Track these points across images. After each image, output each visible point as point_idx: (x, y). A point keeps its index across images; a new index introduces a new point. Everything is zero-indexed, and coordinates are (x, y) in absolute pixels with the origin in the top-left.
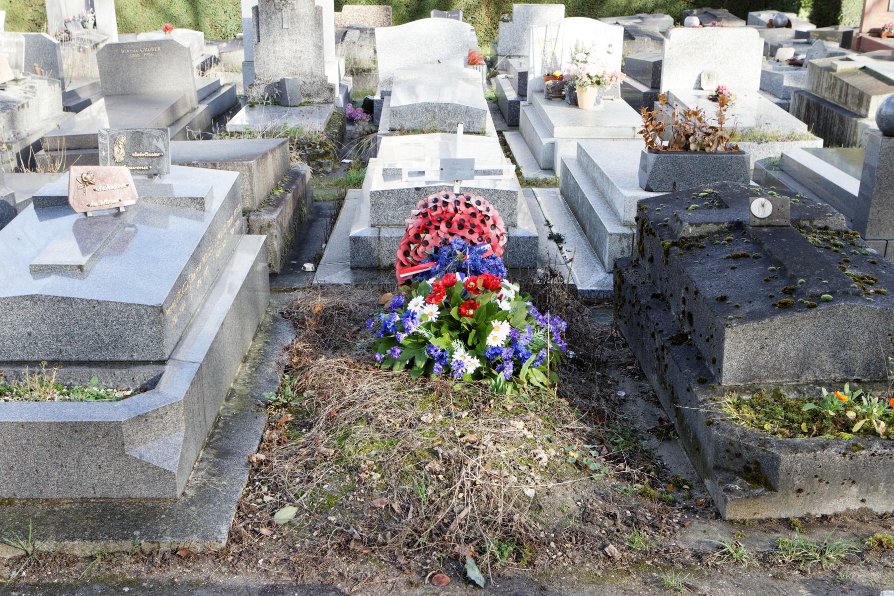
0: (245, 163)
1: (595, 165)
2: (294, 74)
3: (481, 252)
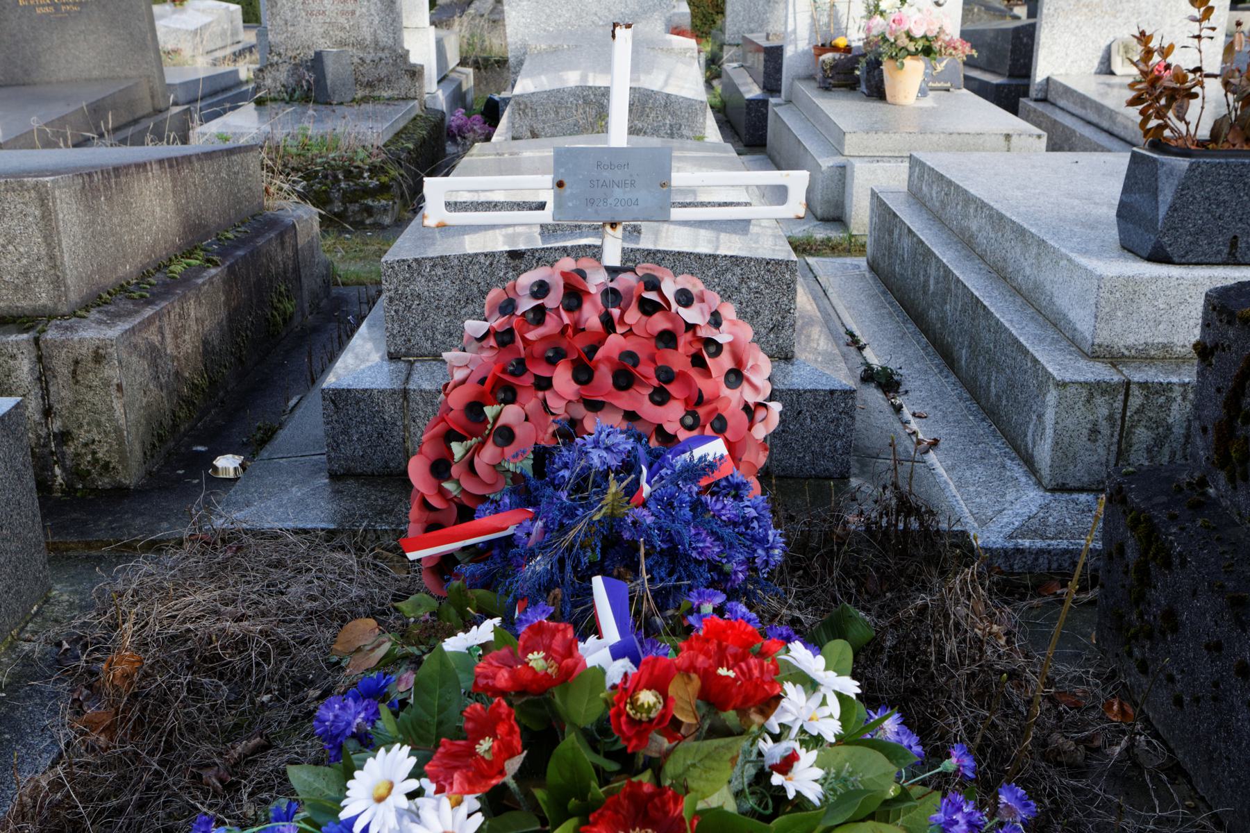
0: (30, 181)
1: (968, 199)
2: (342, 43)
3: (694, 471)
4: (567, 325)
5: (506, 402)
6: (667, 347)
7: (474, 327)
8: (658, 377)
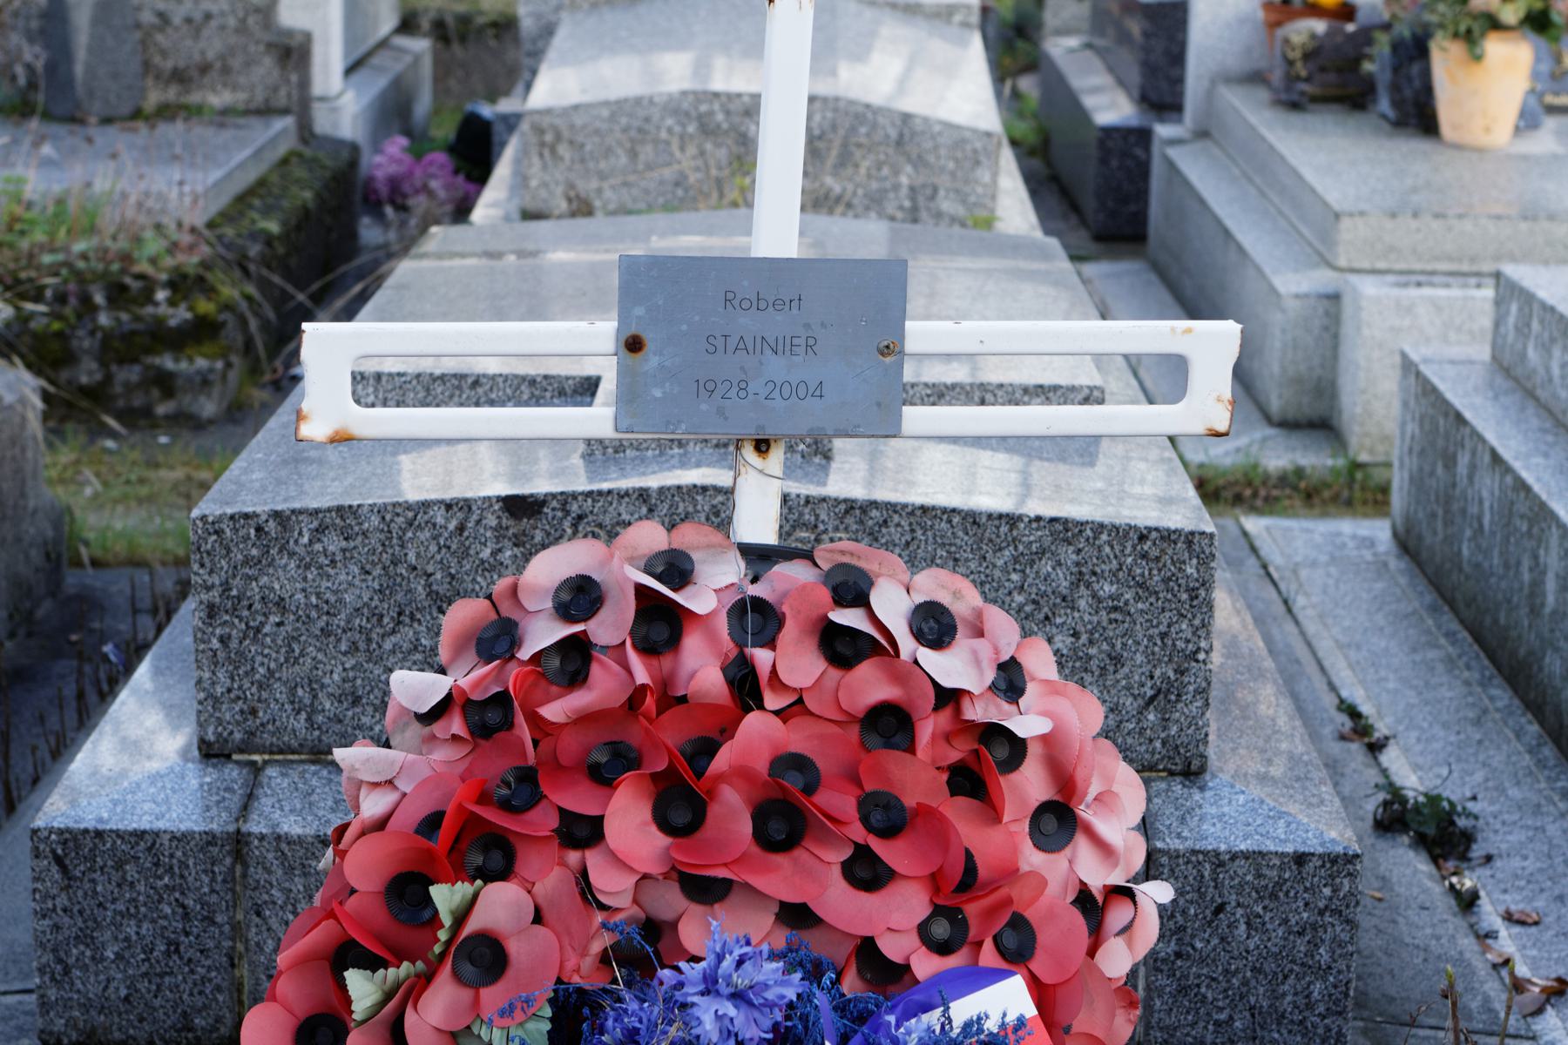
4: (644, 686)
5: (489, 875)
6: (890, 745)
7: (415, 687)
8: (865, 820)
